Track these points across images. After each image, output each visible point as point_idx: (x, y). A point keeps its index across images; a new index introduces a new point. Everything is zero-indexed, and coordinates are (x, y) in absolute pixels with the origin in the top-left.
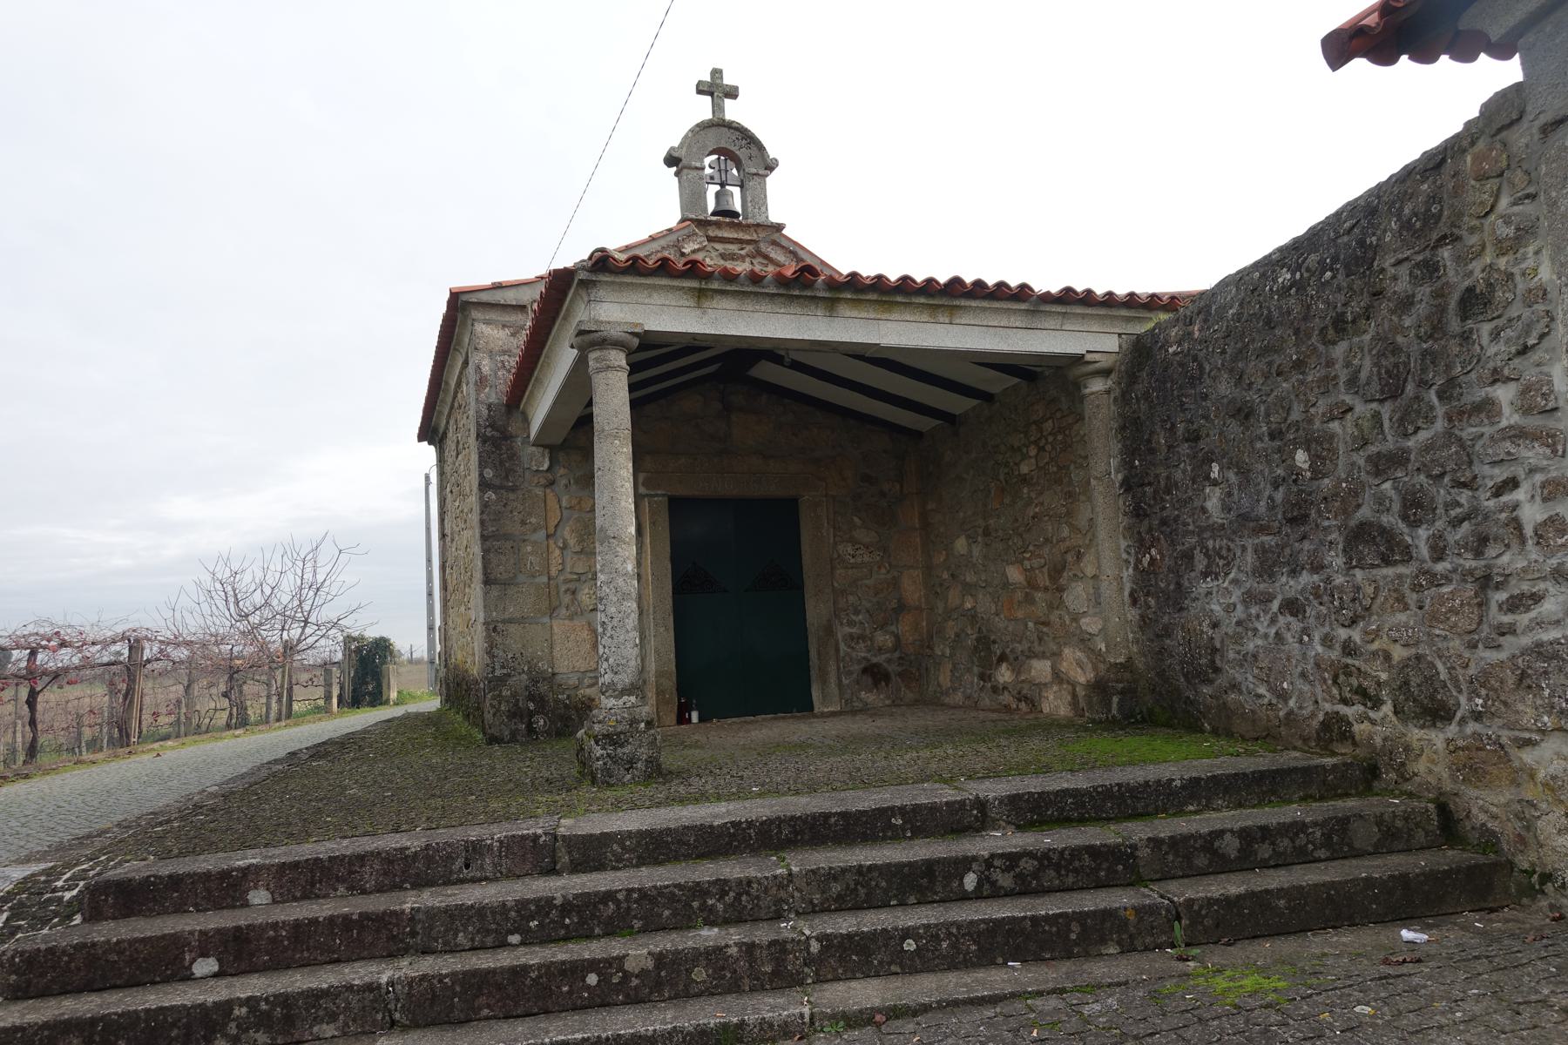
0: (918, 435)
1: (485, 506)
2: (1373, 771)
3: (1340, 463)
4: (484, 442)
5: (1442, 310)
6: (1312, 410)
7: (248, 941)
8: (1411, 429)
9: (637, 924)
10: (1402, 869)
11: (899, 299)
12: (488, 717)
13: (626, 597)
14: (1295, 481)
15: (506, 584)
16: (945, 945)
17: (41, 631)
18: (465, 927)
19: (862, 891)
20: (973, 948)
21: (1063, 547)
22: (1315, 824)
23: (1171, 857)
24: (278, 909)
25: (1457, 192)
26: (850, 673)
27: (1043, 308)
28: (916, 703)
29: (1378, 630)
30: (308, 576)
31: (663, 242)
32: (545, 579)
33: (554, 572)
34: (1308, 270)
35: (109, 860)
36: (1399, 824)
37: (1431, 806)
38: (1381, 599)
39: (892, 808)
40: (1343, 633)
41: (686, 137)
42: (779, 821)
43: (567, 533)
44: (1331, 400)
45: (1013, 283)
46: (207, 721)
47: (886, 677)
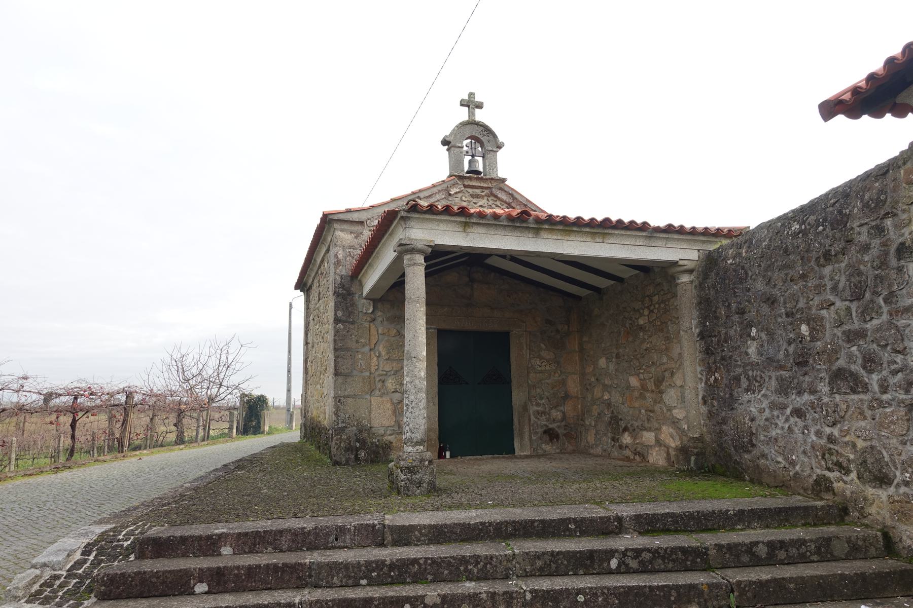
0: (579, 298)
1: (337, 332)
2: (845, 511)
3: (827, 335)
4: (338, 296)
5: (887, 253)
6: (811, 303)
7: (224, 575)
8: (868, 318)
9: (430, 577)
10: (862, 570)
11: (575, 229)
12: (334, 450)
13: (420, 390)
14: (801, 342)
15: (346, 376)
16: (600, 599)
17: (80, 385)
18: (338, 573)
19: (553, 566)
20: (616, 602)
21: (663, 367)
22: (811, 541)
23: (728, 556)
24: (237, 558)
25: (894, 190)
26: (536, 433)
27: (655, 235)
28: (573, 452)
29: (849, 429)
30: (223, 358)
31: (439, 188)
32: (368, 374)
33: (373, 370)
34: (809, 224)
35: (144, 525)
36: (860, 543)
37: (879, 533)
38: (850, 412)
39: (569, 519)
40: (828, 430)
41: (454, 130)
42: (507, 523)
43: (381, 348)
44: (822, 298)
45: (639, 221)
46: (161, 438)
47: (557, 437)
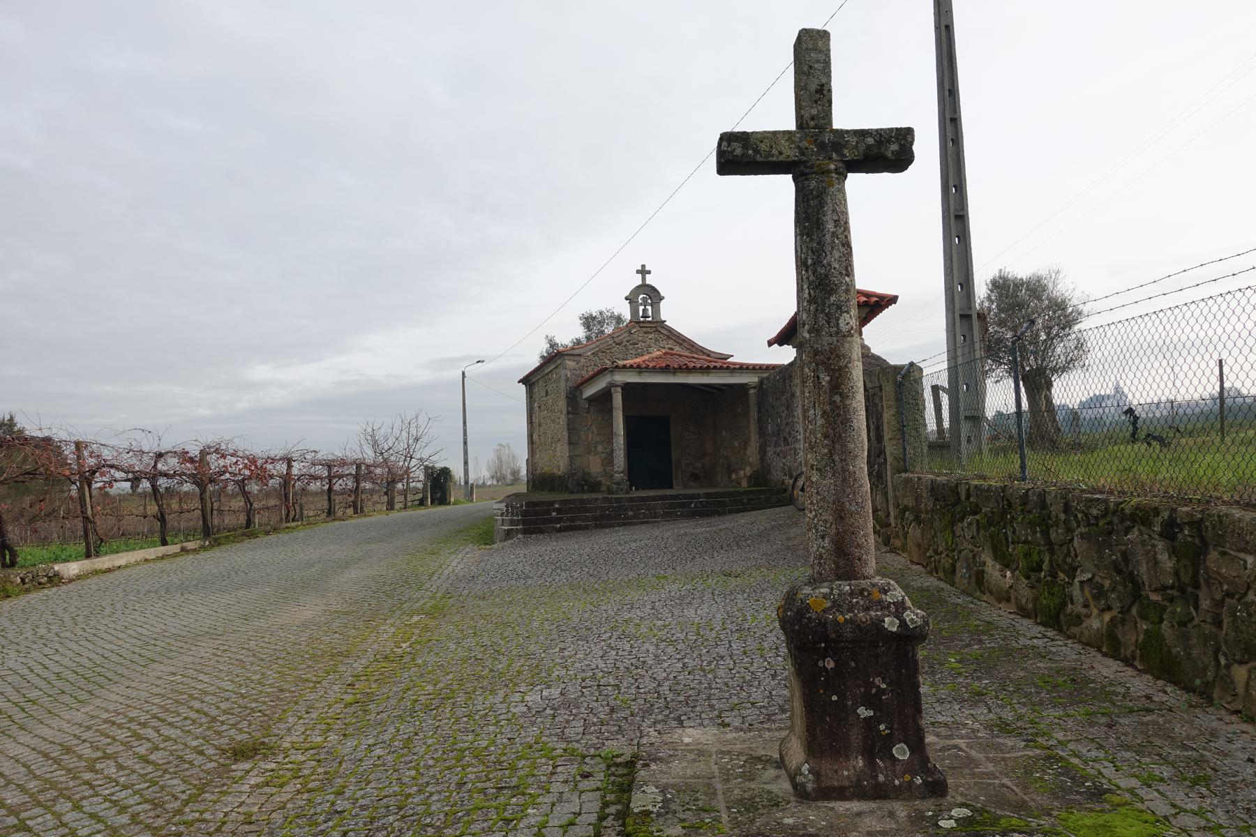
30: (413, 431)
